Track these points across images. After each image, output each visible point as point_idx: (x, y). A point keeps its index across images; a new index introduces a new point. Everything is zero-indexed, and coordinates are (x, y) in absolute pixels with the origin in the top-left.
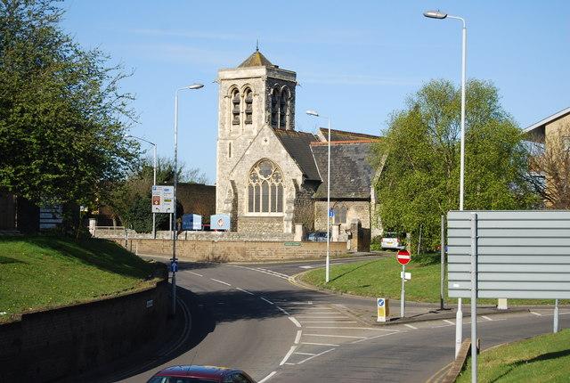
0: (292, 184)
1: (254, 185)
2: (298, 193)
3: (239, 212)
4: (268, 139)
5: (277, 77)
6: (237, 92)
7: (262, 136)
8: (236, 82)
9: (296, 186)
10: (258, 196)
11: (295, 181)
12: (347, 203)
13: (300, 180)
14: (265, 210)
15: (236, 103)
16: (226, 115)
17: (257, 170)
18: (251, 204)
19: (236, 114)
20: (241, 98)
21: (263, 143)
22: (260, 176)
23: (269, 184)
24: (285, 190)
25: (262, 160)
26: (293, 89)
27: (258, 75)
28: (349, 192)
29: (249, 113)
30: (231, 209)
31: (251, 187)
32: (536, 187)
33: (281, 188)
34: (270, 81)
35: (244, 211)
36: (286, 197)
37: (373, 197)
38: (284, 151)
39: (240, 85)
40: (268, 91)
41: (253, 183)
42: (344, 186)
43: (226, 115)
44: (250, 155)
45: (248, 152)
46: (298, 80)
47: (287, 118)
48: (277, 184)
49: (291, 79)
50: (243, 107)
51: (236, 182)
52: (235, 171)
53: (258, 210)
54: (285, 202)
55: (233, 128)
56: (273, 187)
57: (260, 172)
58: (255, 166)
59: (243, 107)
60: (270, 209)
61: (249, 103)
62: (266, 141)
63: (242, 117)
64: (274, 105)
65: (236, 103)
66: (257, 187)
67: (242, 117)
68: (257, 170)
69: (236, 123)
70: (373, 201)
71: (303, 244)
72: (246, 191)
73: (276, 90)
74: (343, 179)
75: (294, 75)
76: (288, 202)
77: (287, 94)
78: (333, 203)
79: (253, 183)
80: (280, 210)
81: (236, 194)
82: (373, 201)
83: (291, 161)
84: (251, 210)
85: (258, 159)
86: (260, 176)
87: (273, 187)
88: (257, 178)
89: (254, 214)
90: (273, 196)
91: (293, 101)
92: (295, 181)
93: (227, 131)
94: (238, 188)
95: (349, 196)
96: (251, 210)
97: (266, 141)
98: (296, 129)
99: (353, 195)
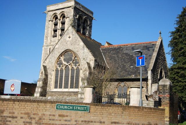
0: (86, 66)
1: (59, 69)
2: (90, 73)
3: (48, 89)
4: (71, 36)
5: (81, 9)
6: (57, 18)
7: (67, 34)
8: (56, 12)
9: (90, 67)
10: (61, 77)
11: (88, 64)
12: (128, 83)
13: (92, 64)
14: (66, 87)
15: (56, 25)
16: (49, 32)
17: (62, 58)
18: (56, 82)
19: (55, 31)
20: (59, 21)
21: (68, 39)
22: (64, 62)
23: (70, 67)
24: (81, 72)
25: (66, 51)
26: (91, 21)
27: (69, 6)
28: (130, 75)
29: (63, 30)
30: (41, 86)
31: (57, 70)
32: (182, 82)
33: (78, 71)
34: (75, 9)
35: (51, 87)
36: (81, 75)
37: (150, 77)
38: (82, 43)
39: (58, 13)
40: (75, 16)
41: (59, 68)
42: (126, 71)
43: (49, 32)
44: (58, 48)
45: (57, 47)
46: (94, 16)
47: (86, 12)
48: (75, 68)
49: (91, 15)
50: (59, 26)
51: (48, 67)
52: (48, 60)
53: (61, 87)
54: (80, 79)
55: (53, 39)
56: (73, 69)
57: (64, 60)
58: (61, 55)
59: (59, 26)
60: (58, 88)
61: (63, 23)
62: (69, 37)
63: (59, 32)
64: (79, 26)
65: (56, 25)
66: (62, 71)
67: (59, 32)
68: (62, 58)
69: (55, 36)
70: (150, 82)
71: (93, 108)
72: (54, 73)
73: (80, 17)
74: (124, 66)
75: (92, 13)
76: (83, 80)
77: (87, 22)
78: (138, 77)
79: (59, 68)
80: (77, 87)
81: (46, 75)
82: (150, 82)
83: (86, 50)
84: (56, 87)
85: (63, 51)
86: (64, 62)
87: (73, 69)
88: (62, 64)
89: (58, 90)
90: (72, 77)
91: (91, 27)
92: (88, 64)
93: (49, 41)
94: (49, 71)
95: (130, 77)
96: (56, 87)
97: (69, 37)
98: (93, 37)
99: (133, 77)
